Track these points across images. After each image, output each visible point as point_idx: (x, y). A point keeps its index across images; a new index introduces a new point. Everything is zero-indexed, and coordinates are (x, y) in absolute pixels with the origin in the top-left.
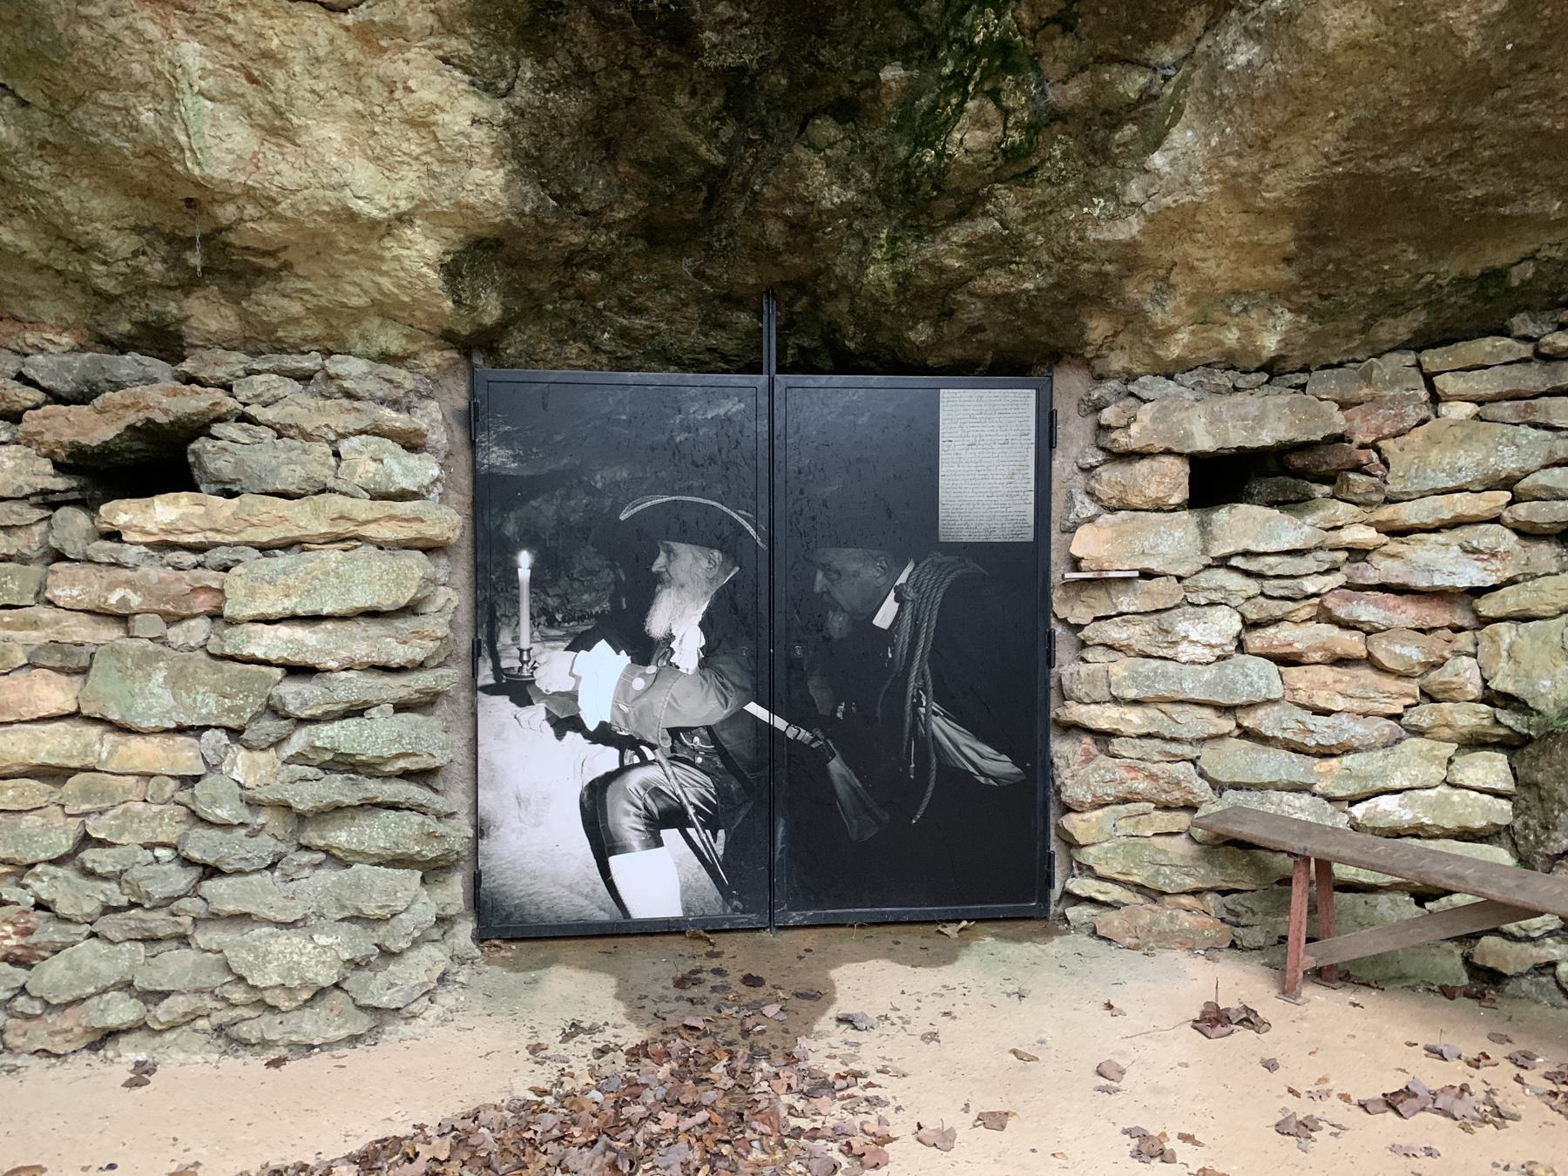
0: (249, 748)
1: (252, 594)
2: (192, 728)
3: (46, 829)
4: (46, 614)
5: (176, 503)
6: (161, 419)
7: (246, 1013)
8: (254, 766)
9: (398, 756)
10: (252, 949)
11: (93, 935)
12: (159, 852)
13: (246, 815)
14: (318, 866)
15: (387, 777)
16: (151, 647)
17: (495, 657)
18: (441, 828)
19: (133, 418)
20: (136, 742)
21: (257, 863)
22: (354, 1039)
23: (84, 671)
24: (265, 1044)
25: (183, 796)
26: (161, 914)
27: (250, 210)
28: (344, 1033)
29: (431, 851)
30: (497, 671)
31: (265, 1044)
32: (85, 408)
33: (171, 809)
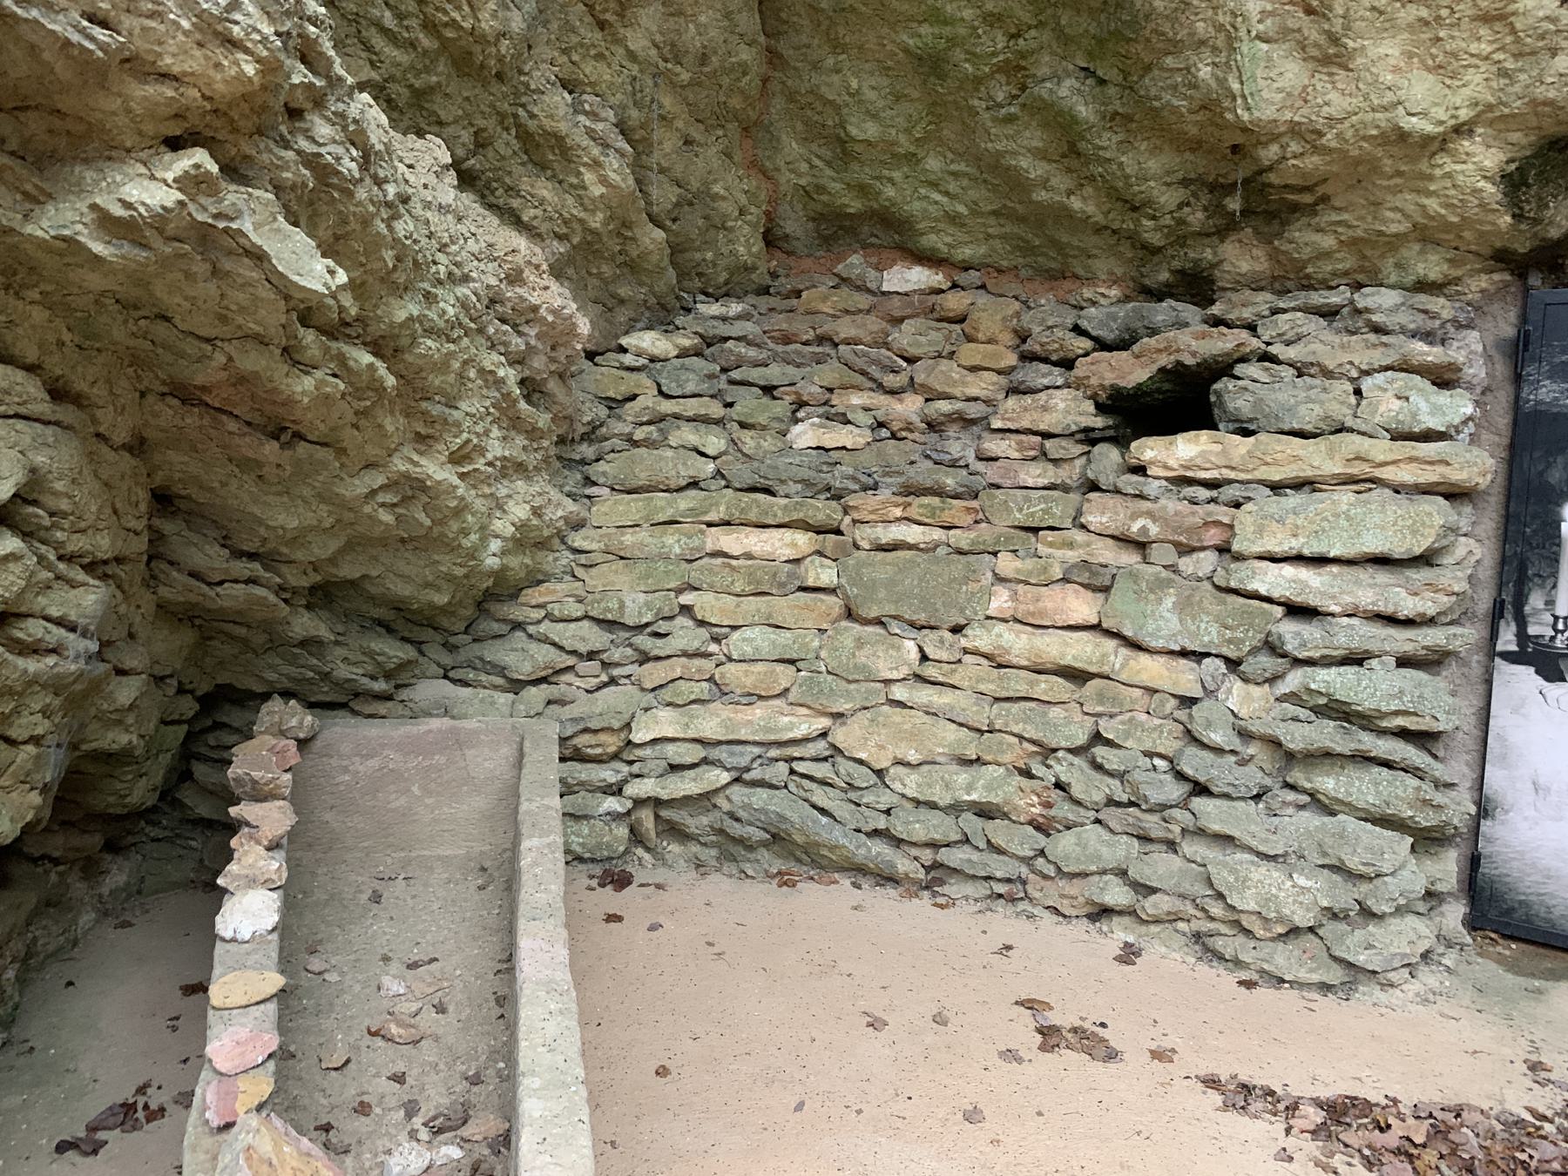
0: (1246, 680)
1: (1260, 531)
2: (1194, 653)
3: (1068, 721)
4: (1080, 536)
5: (1197, 442)
6: (1189, 361)
7: (1224, 929)
8: (1248, 698)
9: (1397, 713)
10: (1233, 871)
11: (1098, 821)
12: (1157, 762)
13: (1236, 743)
14: (1301, 807)
15: (1383, 732)
16: (1165, 574)
17: (1521, 622)
18: (1439, 798)
19: (1165, 360)
20: (1144, 658)
21: (1243, 792)
22: (1325, 988)
23: (1106, 590)
24: (1238, 963)
25: (1182, 715)
26: (1155, 818)
27: (1294, 147)
28: (1315, 978)
29: (1426, 819)
30: (1522, 636)
31: (1238, 963)
32: (1124, 354)
33: (1170, 725)
